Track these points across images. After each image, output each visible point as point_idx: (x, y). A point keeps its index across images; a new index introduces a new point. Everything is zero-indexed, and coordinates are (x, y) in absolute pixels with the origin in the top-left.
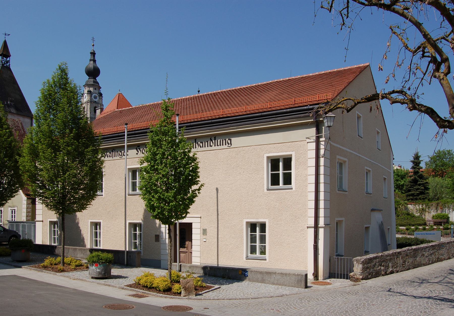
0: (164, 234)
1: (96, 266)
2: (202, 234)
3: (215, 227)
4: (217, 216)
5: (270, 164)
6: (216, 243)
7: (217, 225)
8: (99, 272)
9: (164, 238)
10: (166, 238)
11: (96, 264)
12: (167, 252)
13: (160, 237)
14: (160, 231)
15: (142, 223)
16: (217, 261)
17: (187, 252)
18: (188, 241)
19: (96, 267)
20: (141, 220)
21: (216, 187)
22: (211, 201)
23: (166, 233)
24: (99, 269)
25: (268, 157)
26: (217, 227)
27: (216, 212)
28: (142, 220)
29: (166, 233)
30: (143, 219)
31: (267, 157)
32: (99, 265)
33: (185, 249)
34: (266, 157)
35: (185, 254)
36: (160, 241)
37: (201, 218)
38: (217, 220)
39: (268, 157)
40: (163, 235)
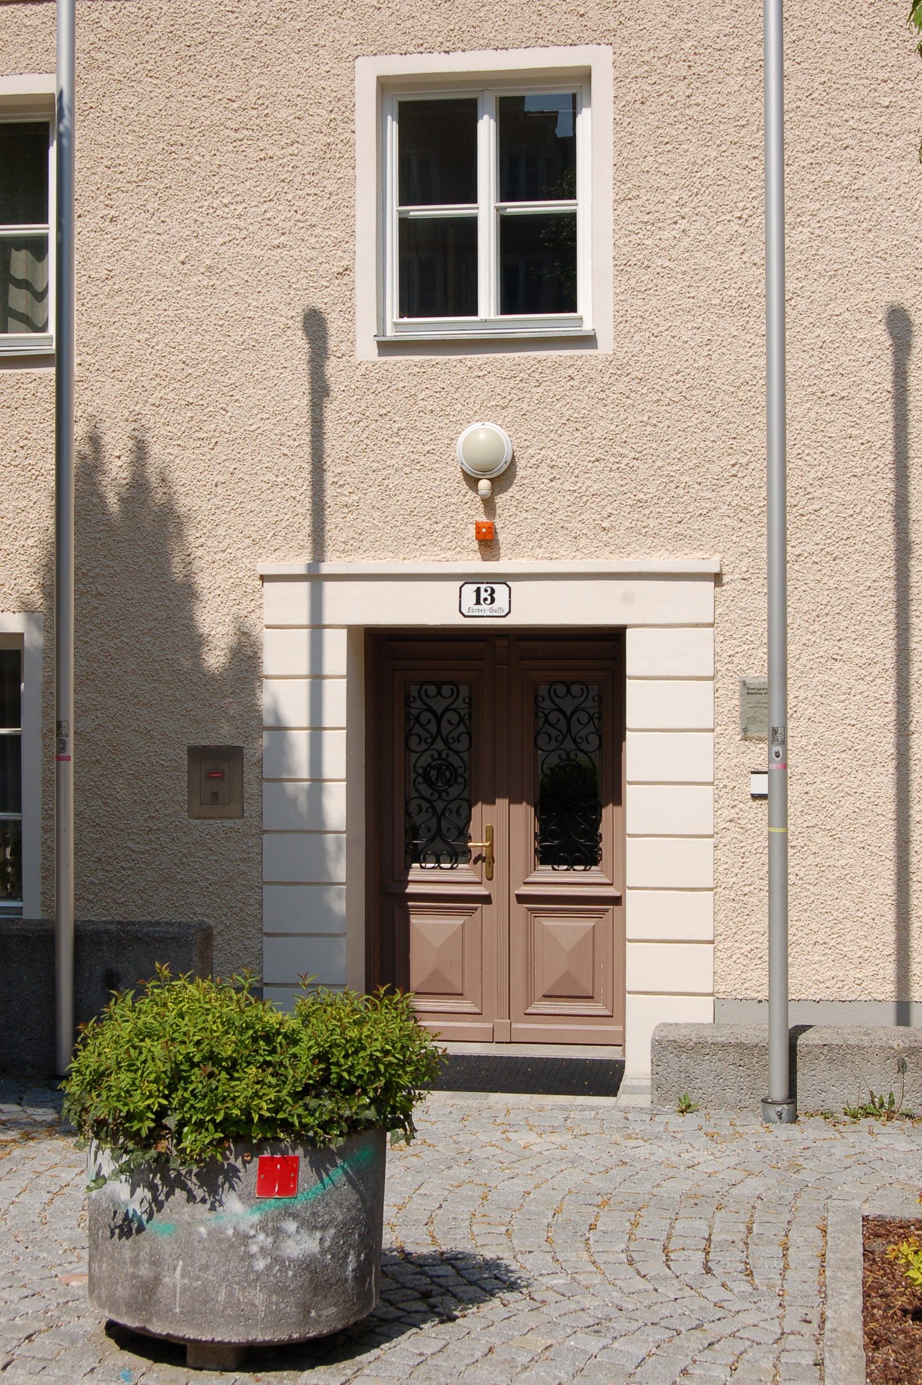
0: (300, 741)
1: (265, 1189)
2: (734, 732)
3: (872, 662)
4: (890, 563)
5: (393, 128)
6: (889, 809)
7: (891, 644)
8: (309, 1266)
9: (303, 771)
10: (317, 780)
11: (263, 1162)
12: (329, 910)
13: (250, 774)
14: (252, 711)
15: (34, 640)
16: (890, 970)
17: (486, 899)
18: (502, 803)
19: (272, 1204)
20: (14, 604)
21: (887, 298)
22: (832, 430)
23: (316, 729)
24: (310, 1224)
25: (385, 85)
26: (888, 657)
27: (889, 527)
28: (27, 609)
29: (316, 729)
30: (37, 599)
31: (378, 77)
32: (304, 1166)
33: (465, 870)
34: (375, 80)
35: (590, 923)
36: (248, 811)
37: (717, 578)
38: (891, 595)
39: (385, 85)
40: (282, 749)
